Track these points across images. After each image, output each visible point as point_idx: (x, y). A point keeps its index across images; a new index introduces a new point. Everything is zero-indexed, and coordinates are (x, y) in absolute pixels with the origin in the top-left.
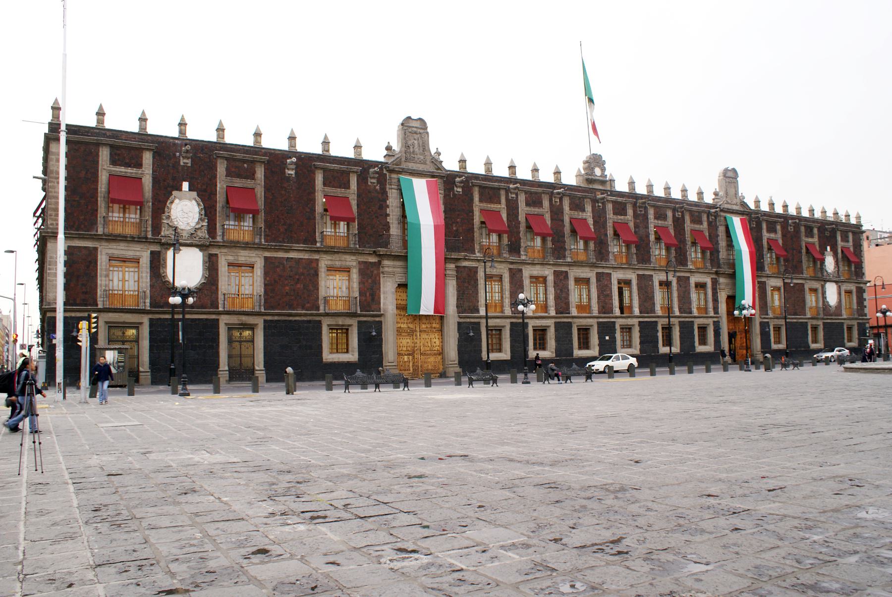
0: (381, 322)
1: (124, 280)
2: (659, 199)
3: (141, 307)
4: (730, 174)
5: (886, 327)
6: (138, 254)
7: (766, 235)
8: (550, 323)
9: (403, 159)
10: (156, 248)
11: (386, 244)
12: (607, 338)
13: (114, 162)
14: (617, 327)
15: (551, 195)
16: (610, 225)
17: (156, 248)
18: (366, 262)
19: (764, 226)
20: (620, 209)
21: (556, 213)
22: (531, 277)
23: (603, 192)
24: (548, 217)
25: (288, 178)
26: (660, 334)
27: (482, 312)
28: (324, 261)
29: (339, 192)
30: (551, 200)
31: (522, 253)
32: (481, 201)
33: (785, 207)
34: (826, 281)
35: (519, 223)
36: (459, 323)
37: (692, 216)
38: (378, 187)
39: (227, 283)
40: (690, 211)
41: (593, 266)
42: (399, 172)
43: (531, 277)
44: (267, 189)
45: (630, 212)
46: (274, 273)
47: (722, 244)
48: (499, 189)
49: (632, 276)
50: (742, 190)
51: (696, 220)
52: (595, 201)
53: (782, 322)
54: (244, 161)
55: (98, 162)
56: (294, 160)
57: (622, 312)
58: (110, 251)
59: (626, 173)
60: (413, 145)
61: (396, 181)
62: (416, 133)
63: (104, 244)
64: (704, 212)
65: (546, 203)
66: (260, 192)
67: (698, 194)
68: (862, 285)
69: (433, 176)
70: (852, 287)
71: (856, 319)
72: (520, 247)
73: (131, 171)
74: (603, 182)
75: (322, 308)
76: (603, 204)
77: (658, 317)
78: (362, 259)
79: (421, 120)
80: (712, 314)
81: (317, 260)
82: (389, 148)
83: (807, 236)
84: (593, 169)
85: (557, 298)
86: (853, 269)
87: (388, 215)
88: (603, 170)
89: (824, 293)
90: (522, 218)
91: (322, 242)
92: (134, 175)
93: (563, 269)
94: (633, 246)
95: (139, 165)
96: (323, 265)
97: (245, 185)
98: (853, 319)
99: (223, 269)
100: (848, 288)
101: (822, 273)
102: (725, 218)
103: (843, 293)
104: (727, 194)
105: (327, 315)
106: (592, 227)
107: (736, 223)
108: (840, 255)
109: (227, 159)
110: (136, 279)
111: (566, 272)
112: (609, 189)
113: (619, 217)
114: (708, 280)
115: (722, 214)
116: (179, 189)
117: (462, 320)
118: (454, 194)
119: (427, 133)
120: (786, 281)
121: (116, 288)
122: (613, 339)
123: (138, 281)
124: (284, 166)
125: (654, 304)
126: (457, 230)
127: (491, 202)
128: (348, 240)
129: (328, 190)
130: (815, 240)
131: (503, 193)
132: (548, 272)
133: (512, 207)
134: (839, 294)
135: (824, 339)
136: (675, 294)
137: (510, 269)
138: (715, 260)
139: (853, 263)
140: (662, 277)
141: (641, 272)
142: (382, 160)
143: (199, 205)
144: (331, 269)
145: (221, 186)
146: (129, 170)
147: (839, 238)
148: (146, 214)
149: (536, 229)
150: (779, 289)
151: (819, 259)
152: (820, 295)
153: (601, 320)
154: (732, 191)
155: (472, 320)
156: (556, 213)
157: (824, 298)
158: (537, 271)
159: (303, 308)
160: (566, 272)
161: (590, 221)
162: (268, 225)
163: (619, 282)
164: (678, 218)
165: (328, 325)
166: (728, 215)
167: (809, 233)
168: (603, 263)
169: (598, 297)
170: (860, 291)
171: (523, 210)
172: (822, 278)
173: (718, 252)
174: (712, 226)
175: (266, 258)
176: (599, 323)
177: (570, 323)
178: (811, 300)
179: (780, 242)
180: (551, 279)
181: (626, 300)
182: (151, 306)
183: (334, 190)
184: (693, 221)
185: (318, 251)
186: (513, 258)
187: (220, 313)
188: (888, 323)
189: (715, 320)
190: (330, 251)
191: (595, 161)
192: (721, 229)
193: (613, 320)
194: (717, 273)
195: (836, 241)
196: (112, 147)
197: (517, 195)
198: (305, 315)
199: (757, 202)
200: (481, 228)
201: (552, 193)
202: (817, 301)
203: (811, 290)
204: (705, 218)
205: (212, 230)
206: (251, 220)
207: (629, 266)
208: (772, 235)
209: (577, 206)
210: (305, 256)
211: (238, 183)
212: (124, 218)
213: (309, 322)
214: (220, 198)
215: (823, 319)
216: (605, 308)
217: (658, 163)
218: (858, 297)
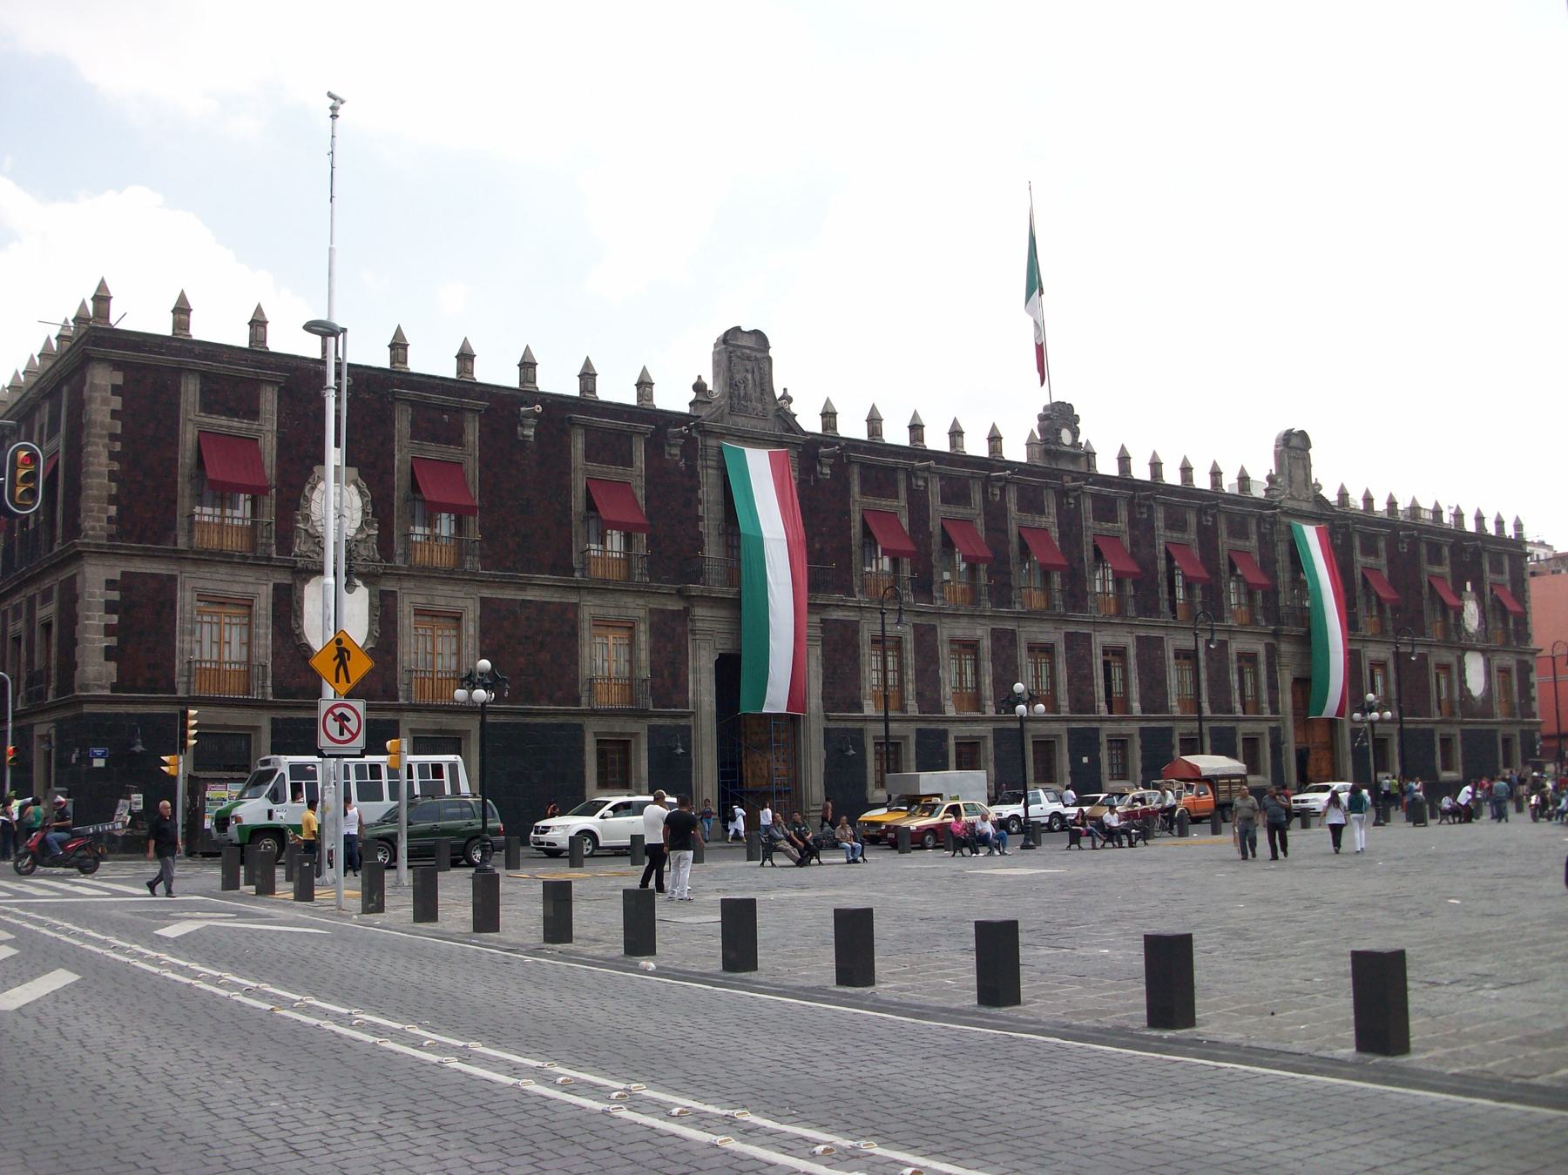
0: (688, 728)
1: (220, 643)
3: (256, 695)
4: (1294, 442)
5: (1561, 736)
6: (251, 589)
7: (1360, 560)
8: (985, 730)
9: (727, 410)
11: (697, 575)
12: (1085, 760)
13: (208, 407)
14: (1103, 739)
15: (987, 482)
16: (1087, 540)
17: (284, 578)
18: (663, 611)
20: (1105, 510)
21: (995, 516)
22: (952, 641)
23: (1077, 476)
24: (980, 524)
25: (524, 443)
27: (869, 709)
28: (590, 608)
29: (614, 472)
30: (985, 492)
31: (936, 594)
32: (863, 493)
33: (956, 433)
34: (1465, 649)
35: (930, 535)
36: (827, 731)
37: (1230, 523)
38: (682, 464)
39: (413, 647)
40: (1229, 514)
41: (1061, 620)
42: (721, 436)
43: (952, 641)
44: (484, 463)
45: (1123, 514)
46: (498, 630)
47: (1284, 577)
48: (895, 469)
49: (1127, 640)
50: (1316, 474)
51: (1239, 531)
52: (1062, 493)
54: (443, 409)
55: (178, 406)
56: (538, 408)
58: (200, 584)
59: (1116, 438)
60: (745, 380)
61: (715, 451)
62: (749, 358)
63: (189, 568)
64: (1251, 514)
65: (977, 497)
66: (472, 469)
67: (823, 415)
68: (1527, 657)
69: (780, 444)
70: (1510, 661)
71: (1518, 723)
73: (237, 425)
74: (1075, 458)
75: (584, 700)
76: (1077, 499)
77: (1174, 719)
78: (655, 603)
79: (759, 335)
80: (1267, 715)
81: (576, 605)
82: (699, 387)
83: (1430, 562)
84: (1058, 432)
86: (1511, 625)
87: (701, 519)
88: (1075, 433)
89: (1462, 672)
90: (935, 526)
91: (406, 555)
92: (243, 433)
93: (1009, 626)
94: (1128, 581)
95: (253, 413)
96: (587, 616)
97: (446, 457)
98: (1510, 723)
99: (406, 622)
101: (1459, 634)
102: (1289, 527)
103: (1495, 672)
105: (416, 709)
106: (642, 503)
107: (759, 465)
108: (1488, 599)
109: (412, 403)
110: (245, 639)
112: (1084, 469)
114: (1260, 648)
115: (1284, 519)
117: (832, 725)
118: (817, 480)
119: (770, 360)
120: (1403, 649)
121: (206, 657)
122: (1095, 762)
124: (517, 420)
125: (1166, 694)
126: (821, 550)
127: (881, 495)
128: (629, 568)
130: (1445, 569)
131: (902, 476)
132: (981, 632)
133: (918, 504)
134: (1488, 674)
135: (1464, 763)
138: (1273, 612)
139: (1508, 620)
140: (1185, 641)
142: (686, 409)
143: (361, 493)
144: (602, 624)
145: (402, 457)
146: (236, 423)
147: (1486, 567)
148: (267, 510)
149: (607, 512)
150: (1382, 665)
151: (1454, 607)
152: (1455, 676)
153: (1074, 725)
154: (1299, 474)
155: (850, 725)
156: (995, 516)
157: (1463, 682)
158: (962, 629)
159: (551, 701)
161: (1055, 533)
162: (488, 535)
164: (1207, 527)
165: (596, 734)
166: (1295, 522)
167: (1436, 558)
168: (1079, 616)
170: (1525, 669)
171: (937, 509)
172: (1460, 644)
174: (1266, 543)
175: (483, 600)
176: (1071, 732)
178: (1439, 687)
179: (1385, 573)
180: (986, 644)
181: (1117, 687)
182: (275, 694)
183: (605, 468)
184: (1233, 533)
185: (577, 589)
186: (923, 605)
187: (400, 709)
188: (1564, 729)
189: (1273, 724)
190: (601, 588)
191: (1059, 417)
193: (1095, 725)
194: (1276, 634)
195: (1482, 571)
196: (205, 377)
197: (926, 481)
198: (555, 713)
200: (586, 520)
203: (1032, 648)
204: (1253, 527)
205: (385, 544)
206: (248, 504)
208: (1371, 561)
209: (1031, 504)
210: (555, 597)
211: (433, 451)
212: (223, 517)
213: (561, 726)
214: (400, 480)
215: (1462, 723)
216: (1082, 703)
217: (1171, 422)
218: (1520, 680)
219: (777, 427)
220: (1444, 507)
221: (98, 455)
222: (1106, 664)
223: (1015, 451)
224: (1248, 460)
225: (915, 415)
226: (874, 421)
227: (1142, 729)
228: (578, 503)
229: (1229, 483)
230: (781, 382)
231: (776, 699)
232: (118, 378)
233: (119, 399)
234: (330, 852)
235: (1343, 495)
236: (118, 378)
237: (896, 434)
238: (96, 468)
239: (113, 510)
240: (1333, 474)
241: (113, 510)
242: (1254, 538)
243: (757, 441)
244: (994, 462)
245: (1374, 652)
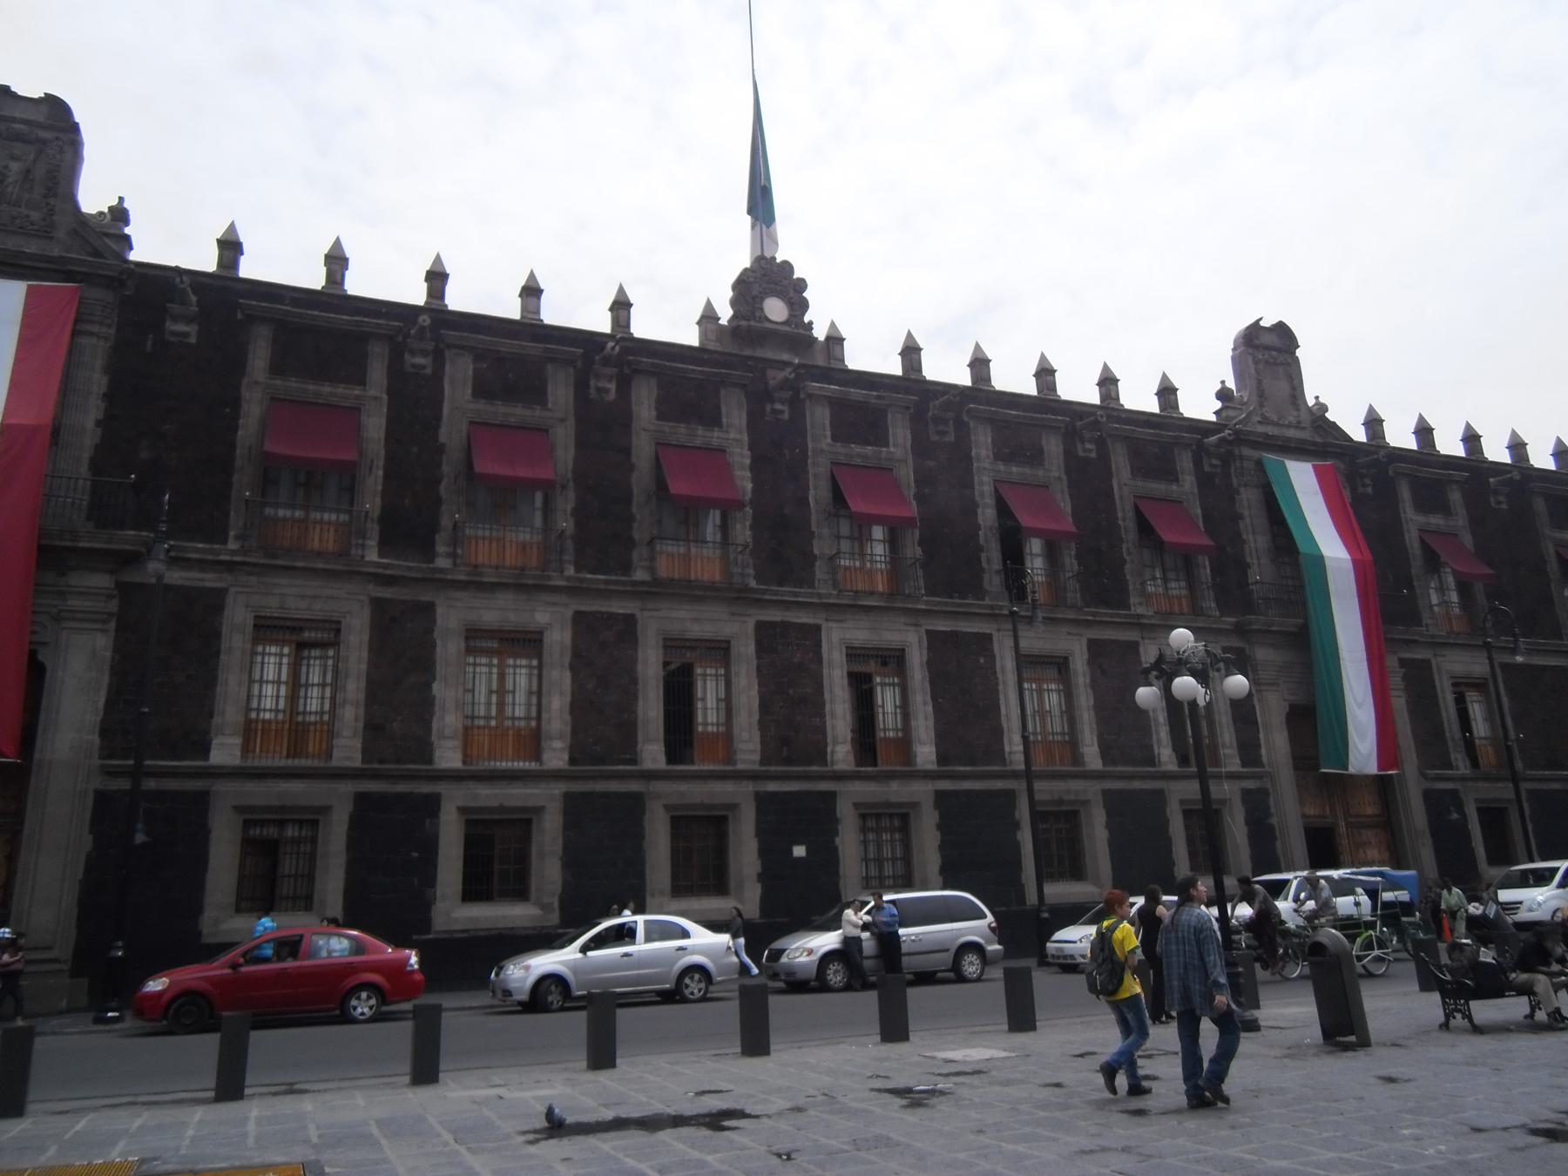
2: (1076, 411)
8: (548, 798)
19: (1405, 493)
26: (1026, 838)
30: (581, 386)
31: (441, 549)
41: (739, 597)
47: (1256, 541)
50: (1314, 388)
52: (758, 397)
53: (1504, 791)
57: (673, 755)
59: (867, 318)
72: (434, 528)
76: (796, 403)
85: (580, 707)
88: (798, 304)
93: (618, 607)
102: (1260, 464)
104: (1261, 395)
111: (630, 620)
113: (856, 449)
115: (1247, 451)
119: (1297, 361)
122: (826, 858)
123: (251, 681)
129: (715, 437)
136: (1085, 699)
137: (378, 605)
141: (943, 626)
142: (1213, 418)
144: (266, 629)
150: (1479, 685)
153: (772, 787)
160: (630, 620)
163: (854, 654)
166: (1269, 457)
168: (786, 592)
169: (764, 707)
173: (1243, 567)
176: (762, 800)
177: (1161, 792)
179: (1467, 540)
181: (708, 714)
184: (1422, 506)
189: (1250, 784)
191: (768, 280)
192: (1248, 500)
194: (1241, 631)
201: (1200, 445)
204: (1185, 462)
207: (894, 601)
208: (1436, 520)
211: (680, 432)
219: (1321, 440)
222: (1460, 701)
223: (1199, 405)
225: (438, 260)
227: (1105, 793)
228: (818, 494)
231: (1363, 753)
240: (1339, 387)
243: (1300, 450)
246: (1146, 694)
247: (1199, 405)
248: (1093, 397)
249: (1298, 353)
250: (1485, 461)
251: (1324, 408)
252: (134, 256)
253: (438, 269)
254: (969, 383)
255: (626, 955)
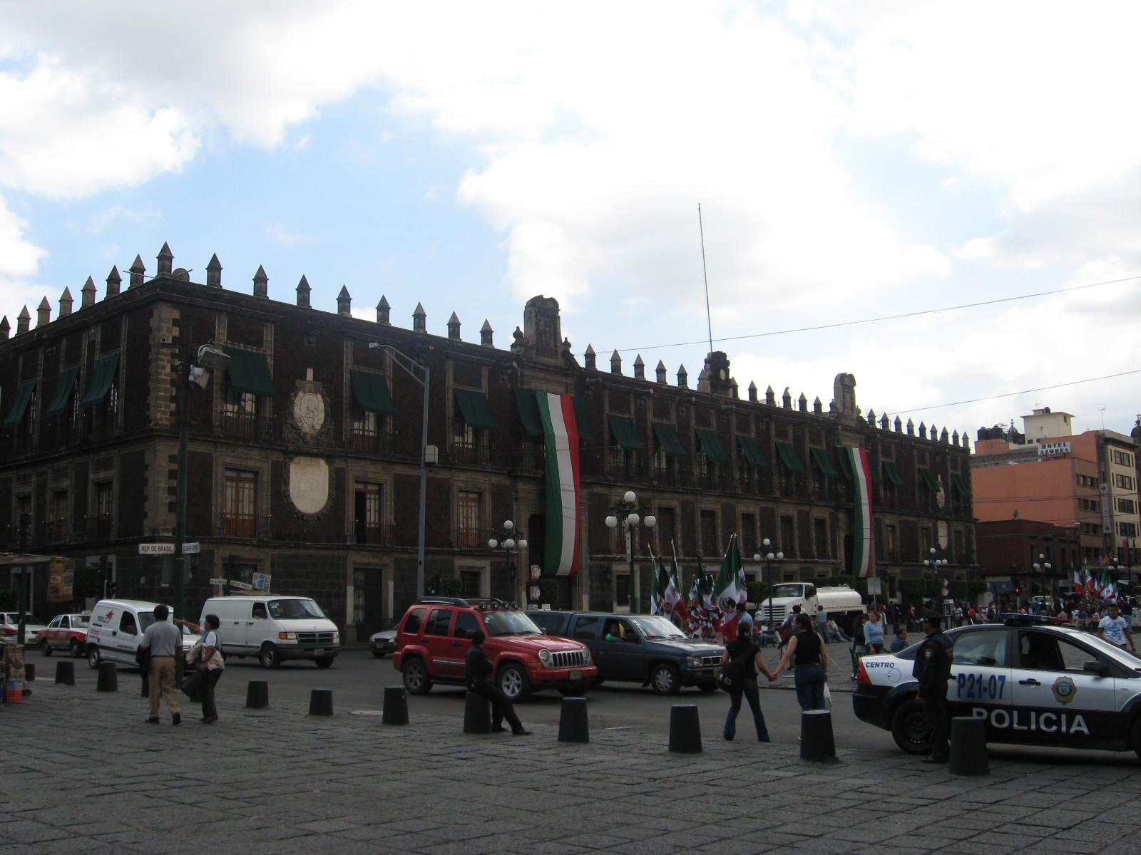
4: (847, 382)
10: (277, 457)
28: (223, 458)
34: (937, 519)
50: (860, 402)
59: (754, 375)
67: (378, 309)
78: (495, 479)
88: (727, 372)
100: (710, 507)
103: (953, 534)
116: (304, 377)
131: (632, 399)
142: (509, 349)
199: (590, 356)
202: (479, 518)
220: (948, 431)
221: (164, 368)
223: (504, 342)
224: (822, 394)
226: (419, 317)
229: (761, 397)
230: (565, 333)
232: (176, 314)
233: (177, 329)
234: (306, 650)
235: (871, 415)
236: (176, 314)
237: (437, 327)
238: (163, 377)
239: (173, 406)
240: (867, 401)
241: (173, 406)
242: (824, 444)
244: (485, 351)
245: (889, 520)
246: (611, 520)
247: (504, 342)
248: (248, 289)
249: (855, 388)
250: (739, 400)
251: (569, 345)
252: (190, 281)
253: (590, 352)
254: (205, 283)
255: (1031, 682)
